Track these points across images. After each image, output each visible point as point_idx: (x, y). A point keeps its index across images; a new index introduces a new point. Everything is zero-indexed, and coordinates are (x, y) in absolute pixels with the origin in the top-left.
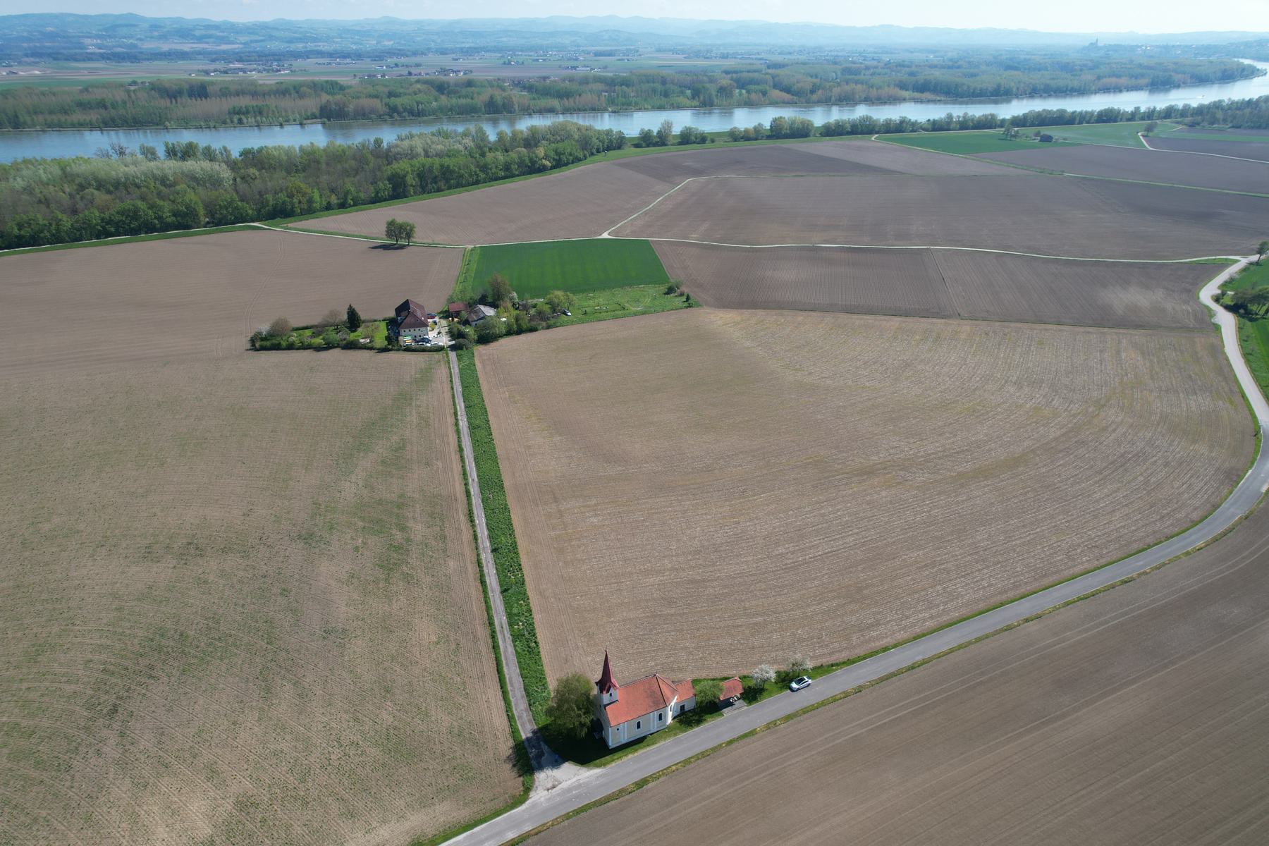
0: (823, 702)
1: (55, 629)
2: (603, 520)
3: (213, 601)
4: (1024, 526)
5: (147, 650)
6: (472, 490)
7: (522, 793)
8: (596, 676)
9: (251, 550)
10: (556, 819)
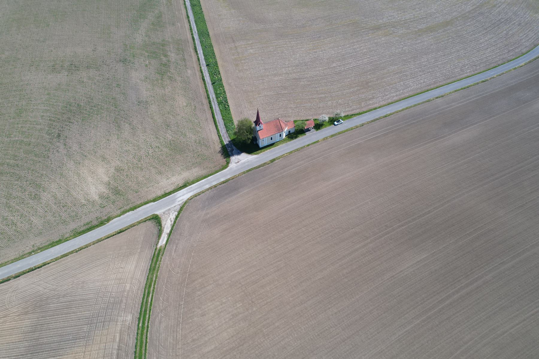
0: (347, 130)
1: (24, 103)
2: (255, 51)
3: (88, 90)
4: (444, 55)
5: (65, 111)
6: (195, 37)
7: (226, 164)
8: (254, 119)
9: (99, 67)
10: (240, 173)
